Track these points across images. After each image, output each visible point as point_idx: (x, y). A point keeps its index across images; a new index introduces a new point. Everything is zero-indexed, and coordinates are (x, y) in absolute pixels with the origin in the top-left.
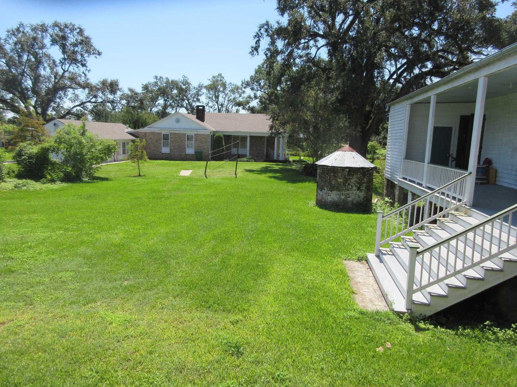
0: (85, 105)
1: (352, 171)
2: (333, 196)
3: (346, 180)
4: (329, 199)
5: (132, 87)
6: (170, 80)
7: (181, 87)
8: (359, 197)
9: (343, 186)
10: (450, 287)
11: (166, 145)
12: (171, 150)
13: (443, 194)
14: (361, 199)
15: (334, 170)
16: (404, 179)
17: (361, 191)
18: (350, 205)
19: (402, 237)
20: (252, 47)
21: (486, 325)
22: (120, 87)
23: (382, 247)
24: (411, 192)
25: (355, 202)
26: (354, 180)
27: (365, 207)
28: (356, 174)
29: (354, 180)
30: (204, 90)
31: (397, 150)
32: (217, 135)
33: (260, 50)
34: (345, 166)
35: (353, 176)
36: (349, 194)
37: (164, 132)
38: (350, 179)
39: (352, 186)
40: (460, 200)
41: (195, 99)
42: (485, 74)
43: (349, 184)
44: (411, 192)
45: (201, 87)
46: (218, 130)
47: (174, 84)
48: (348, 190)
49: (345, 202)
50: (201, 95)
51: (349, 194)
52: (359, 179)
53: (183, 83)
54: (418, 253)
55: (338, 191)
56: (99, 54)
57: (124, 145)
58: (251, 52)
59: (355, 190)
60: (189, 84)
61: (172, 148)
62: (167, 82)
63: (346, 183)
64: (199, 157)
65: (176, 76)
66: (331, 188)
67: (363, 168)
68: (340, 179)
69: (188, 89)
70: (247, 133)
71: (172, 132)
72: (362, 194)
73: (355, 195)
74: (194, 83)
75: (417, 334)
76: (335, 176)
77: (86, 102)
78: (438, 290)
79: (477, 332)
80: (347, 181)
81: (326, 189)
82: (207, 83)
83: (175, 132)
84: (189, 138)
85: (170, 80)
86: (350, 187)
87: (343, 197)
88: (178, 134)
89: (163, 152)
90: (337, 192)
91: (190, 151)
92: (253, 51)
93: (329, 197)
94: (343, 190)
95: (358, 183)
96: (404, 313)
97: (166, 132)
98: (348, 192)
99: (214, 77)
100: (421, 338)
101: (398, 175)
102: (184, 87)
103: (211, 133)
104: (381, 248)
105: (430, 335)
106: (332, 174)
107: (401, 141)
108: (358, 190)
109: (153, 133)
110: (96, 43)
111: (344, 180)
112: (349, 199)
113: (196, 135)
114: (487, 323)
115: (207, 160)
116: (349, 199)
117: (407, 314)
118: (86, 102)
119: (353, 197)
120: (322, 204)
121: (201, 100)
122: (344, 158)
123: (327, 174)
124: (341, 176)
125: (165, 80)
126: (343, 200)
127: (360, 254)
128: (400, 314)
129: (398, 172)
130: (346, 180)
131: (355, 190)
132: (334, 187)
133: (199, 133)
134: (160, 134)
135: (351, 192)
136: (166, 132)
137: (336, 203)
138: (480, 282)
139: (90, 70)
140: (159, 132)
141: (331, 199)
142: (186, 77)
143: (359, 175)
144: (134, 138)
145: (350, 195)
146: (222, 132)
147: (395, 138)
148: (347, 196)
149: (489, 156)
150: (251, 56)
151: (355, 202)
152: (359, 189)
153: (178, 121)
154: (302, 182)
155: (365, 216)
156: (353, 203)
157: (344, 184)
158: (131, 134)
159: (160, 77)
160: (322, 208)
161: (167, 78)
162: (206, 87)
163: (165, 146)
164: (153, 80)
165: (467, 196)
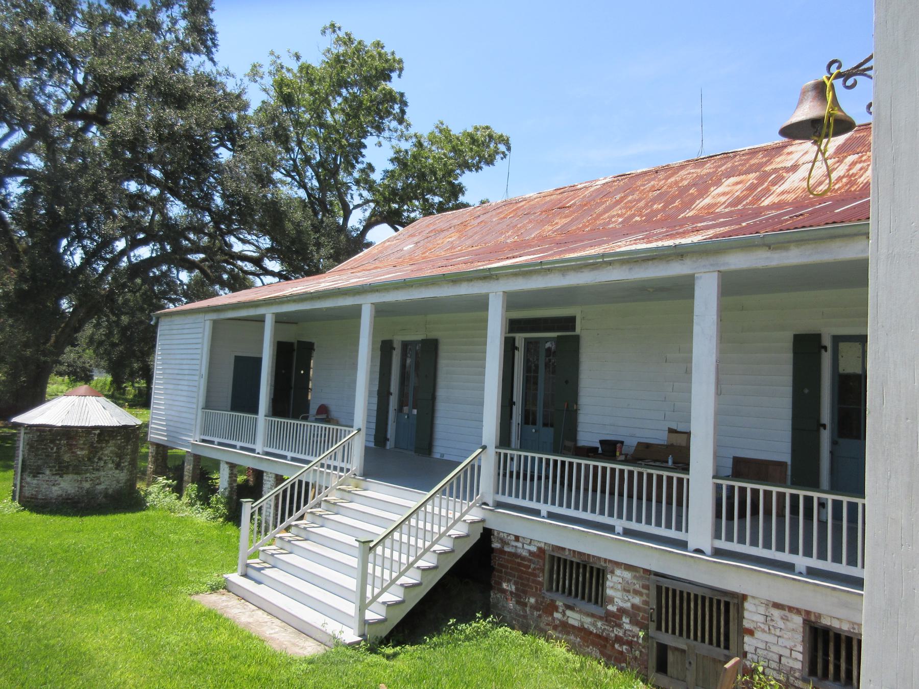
1: (105, 433)
2: (66, 485)
3: (94, 451)
4: (56, 491)
8: (118, 482)
9: (88, 463)
10: (407, 587)
13: (322, 466)
15: (68, 433)
16: (204, 441)
19: (278, 535)
21: (451, 625)
23: (250, 558)
24: (227, 463)
25: (110, 491)
27: (127, 501)
28: (114, 438)
29: (109, 449)
31: (185, 393)
34: (92, 424)
35: (107, 442)
36: (98, 478)
38: (102, 448)
39: (105, 463)
40: (348, 470)
42: (374, 301)
43: (100, 459)
44: (227, 463)
48: (98, 470)
49: (90, 494)
51: (98, 478)
52: (119, 447)
54: (371, 549)
55: (77, 473)
59: (111, 469)
63: (94, 457)
66: (60, 468)
67: (125, 427)
68: (82, 449)
72: (123, 476)
73: (109, 478)
75: (392, 663)
76: (71, 445)
78: (390, 597)
79: (445, 637)
80: (97, 452)
81: (48, 472)
86: (102, 463)
87: (87, 485)
90: (76, 477)
93: (54, 488)
94: (87, 471)
95: (117, 455)
96: (358, 643)
98: (97, 474)
100: (398, 664)
101: (190, 436)
104: (249, 561)
105: (408, 658)
107: (196, 378)
108: (116, 469)
111: (91, 452)
112: (98, 487)
114: (451, 621)
117: (363, 643)
119: (107, 483)
120: (35, 504)
122: (70, 407)
123: (52, 441)
124: (84, 444)
126: (88, 491)
127: (214, 578)
128: (352, 645)
129: (191, 431)
131: (111, 469)
132: (67, 467)
135: (103, 473)
138: (434, 572)
141: (60, 492)
143: (120, 440)
145: (102, 480)
147: (176, 372)
148: (96, 481)
149: (323, 402)
151: (110, 491)
152: (118, 466)
155: (139, 515)
156: (106, 495)
157: (89, 459)
160: (43, 513)
165: (356, 462)
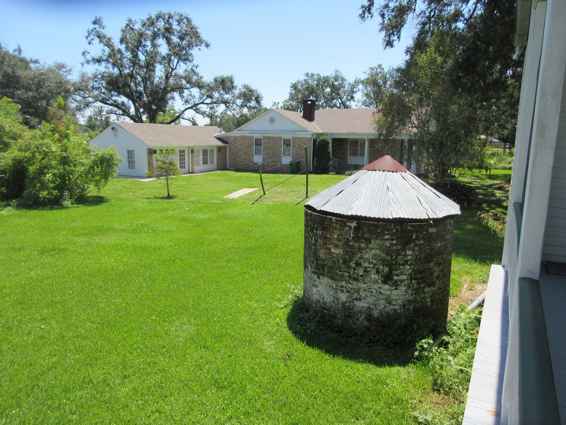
0: (199, 106)
5: (247, 83)
6: (322, 77)
7: (333, 84)
9: (344, 268)
11: (258, 153)
12: (264, 159)
14: (397, 307)
17: (396, 285)
18: (362, 320)
20: (363, 7)
22: (235, 84)
25: (375, 313)
26: (372, 253)
29: (372, 253)
30: (361, 87)
32: (321, 138)
33: (373, 10)
35: (368, 241)
37: (256, 136)
38: (360, 250)
39: (366, 271)
41: (349, 97)
43: (358, 264)
45: (357, 82)
46: (326, 131)
47: (325, 81)
48: (356, 279)
50: (356, 92)
53: (335, 79)
55: (332, 278)
56: (207, 46)
57: (205, 152)
58: (360, 15)
60: (343, 80)
61: (266, 156)
62: (319, 80)
63: (351, 260)
64: (295, 169)
65: (326, 72)
68: (336, 246)
69: (341, 86)
70: (364, 134)
71: (266, 135)
74: (350, 79)
76: (326, 238)
77: (199, 104)
80: (354, 254)
82: (364, 77)
83: (269, 135)
84: (287, 143)
85: (322, 77)
87: (343, 297)
88: (272, 138)
89: (255, 162)
91: (286, 160)
92: (364, 12)
95: (384, 262)
97: (258, 135)
98: (354, 285)
99: (372, 69)
102: (336, 83)
103: (313, 135)
106: (319, 232)
108: (385, 282)
109: (243, 137)
110: (204, 35)
111: (346, 253)
113: (294, 139)
115: (307, 173)
116: (361, 305)
118: (199, 104)
119: (371, 300)
121: (356, 98)
125: (315, 77)
130: (351, 252)
133: (298, 136)
134: (251, 138)
135: (363, 286)
136: (258, 135)
137: (329, 310)
139: (198, 66)
140: (251, 135)
142: (339, 72)
144: (221, 144)
146: (331, 135)
150: (361, 21)
151: (375, 313)
152: (387, 279)
153: (272, 121)
154: (400, 218)
157: (345, 262)
158: (220, 139)
159: (312, 74)
161: (318, 75)
162: (362, 82)
163: (258, 154)
164: (302, 78)
